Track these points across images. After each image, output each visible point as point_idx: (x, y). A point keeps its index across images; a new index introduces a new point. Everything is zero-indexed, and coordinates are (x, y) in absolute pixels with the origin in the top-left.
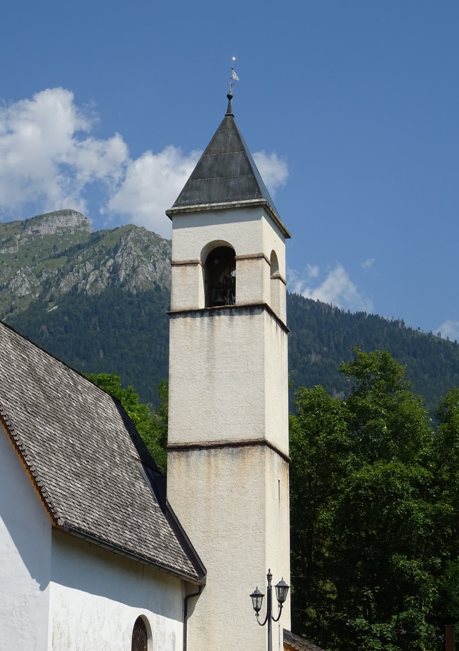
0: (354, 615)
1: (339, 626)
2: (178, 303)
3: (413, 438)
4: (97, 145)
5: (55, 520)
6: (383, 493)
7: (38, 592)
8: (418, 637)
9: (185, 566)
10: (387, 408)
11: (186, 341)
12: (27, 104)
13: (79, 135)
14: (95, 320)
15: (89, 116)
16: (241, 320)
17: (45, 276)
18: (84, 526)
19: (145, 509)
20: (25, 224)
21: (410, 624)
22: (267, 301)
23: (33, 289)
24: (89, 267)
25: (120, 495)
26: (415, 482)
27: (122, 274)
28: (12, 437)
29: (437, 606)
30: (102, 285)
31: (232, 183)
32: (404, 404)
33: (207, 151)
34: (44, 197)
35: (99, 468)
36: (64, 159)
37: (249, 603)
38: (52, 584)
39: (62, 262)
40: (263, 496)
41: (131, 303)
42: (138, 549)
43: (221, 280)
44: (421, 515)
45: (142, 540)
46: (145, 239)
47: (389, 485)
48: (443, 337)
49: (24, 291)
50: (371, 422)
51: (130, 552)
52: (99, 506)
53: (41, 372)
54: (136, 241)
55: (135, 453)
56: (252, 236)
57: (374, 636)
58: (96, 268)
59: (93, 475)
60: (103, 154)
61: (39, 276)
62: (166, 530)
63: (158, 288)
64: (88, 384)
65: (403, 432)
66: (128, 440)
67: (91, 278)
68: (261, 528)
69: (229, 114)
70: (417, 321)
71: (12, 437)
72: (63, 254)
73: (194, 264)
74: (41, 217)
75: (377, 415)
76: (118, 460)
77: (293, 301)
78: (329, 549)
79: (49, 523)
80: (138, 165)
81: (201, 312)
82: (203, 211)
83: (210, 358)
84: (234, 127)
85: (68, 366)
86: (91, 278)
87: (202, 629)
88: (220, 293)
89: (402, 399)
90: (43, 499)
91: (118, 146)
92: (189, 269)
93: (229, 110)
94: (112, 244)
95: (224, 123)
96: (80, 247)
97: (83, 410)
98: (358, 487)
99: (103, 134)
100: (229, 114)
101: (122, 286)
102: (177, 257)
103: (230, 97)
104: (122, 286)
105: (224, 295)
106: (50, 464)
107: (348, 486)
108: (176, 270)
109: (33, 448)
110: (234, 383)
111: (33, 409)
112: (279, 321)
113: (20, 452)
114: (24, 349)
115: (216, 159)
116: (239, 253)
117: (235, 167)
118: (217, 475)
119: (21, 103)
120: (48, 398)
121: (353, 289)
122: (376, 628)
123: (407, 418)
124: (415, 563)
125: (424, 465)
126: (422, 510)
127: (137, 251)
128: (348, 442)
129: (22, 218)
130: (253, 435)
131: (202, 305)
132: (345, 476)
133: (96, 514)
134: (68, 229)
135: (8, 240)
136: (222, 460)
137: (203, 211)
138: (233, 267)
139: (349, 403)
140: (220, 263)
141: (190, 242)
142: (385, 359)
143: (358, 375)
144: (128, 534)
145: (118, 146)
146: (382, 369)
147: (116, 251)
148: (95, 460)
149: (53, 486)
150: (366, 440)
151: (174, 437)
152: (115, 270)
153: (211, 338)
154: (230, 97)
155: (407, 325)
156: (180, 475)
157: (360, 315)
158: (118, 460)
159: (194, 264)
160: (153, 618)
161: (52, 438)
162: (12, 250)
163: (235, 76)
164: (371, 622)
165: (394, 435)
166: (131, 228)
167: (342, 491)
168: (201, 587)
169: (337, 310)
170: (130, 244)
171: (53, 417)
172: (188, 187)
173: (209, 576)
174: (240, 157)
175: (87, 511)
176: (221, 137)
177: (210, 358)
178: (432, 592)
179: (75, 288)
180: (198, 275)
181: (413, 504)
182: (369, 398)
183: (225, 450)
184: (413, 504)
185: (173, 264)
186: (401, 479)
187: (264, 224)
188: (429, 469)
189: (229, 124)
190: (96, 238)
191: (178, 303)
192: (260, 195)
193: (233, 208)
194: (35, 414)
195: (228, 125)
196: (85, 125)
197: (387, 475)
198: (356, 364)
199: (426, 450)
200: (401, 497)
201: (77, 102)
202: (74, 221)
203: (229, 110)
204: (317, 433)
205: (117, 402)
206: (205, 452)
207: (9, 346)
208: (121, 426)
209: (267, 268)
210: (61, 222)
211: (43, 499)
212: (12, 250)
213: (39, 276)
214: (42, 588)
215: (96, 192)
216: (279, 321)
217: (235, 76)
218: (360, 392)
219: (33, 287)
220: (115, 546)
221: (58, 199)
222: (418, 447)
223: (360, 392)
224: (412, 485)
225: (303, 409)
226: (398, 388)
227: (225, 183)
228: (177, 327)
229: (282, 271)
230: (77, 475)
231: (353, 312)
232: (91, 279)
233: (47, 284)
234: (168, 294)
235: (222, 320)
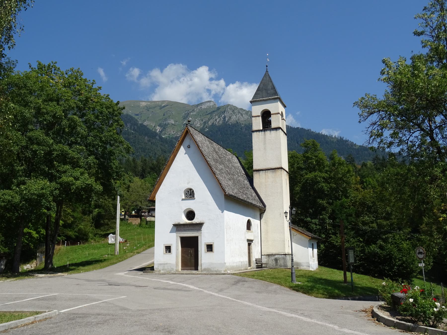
0: (306, 217)
1: (302, 220)
2: (254, 128)
3: (323, 165)
4: (217, 82)
5: (225, 193)
6: (315, 182)
7: (221, 214)
8: (326, 223)
9: (261, 205)
10: (315, 156)
11: (257, 139)
12: (195, 71)
13: (211, 79)
14: (219, 133)
15: (214, 73)
16: (273, 132)
17: (204, 121)
18: (233, 194)
19: (248, 188)
20: (198, 105)
21: (323, 219)
22: (281, 126)
23: (201, 124)
24: (217, 117)
25: (241, 185)
26: (324, 178)
27: (227, 119)
28: (211, 169)
29: (332, 214)
30: (221, 122)
31: (269, 92)
32: (319, 155)
33: (261, 83)
34: (201, 98)
35: (235, 177)
36: (207, 87)
37: (284, 215)
38: (225, 211)
39: (209, 116)
40: (282, 184)
41: (230, 127)
42: (248, 200)
43: (267, 121)
44: (326, 188)
45: (248, 198)
46: (233, 108)
47: (316, 179)
48: (323, 134)
49: (198, 125)
50: (310, 161)
51: (246, 201)
52: (236, 188)
53: (217, 150)
54: (230, 109)
55: (244, 172)
56: (275, 107)
57: (313, 223)
58: (219, 117)
59: (233, 179)
60: (217, 85)
61: (202, 121)
62: (254, 194)
63: (237, 123)
64: (229, 153)
65: (320, 163)
66: (241, 169)
67: (218, 121)
68: (282, 193)
69: (267, 71)
70: (315, 129)
71: (211, 169)
72: (209, 114)
73: (259, 116)
74: (202, 103)
75: (311, 159)
76: (239, 174)
77: (287, 127)
78: (298, 198)
79: (224, 193)
80: (228, 88)
81: (261, 131)
82: (261, 101)
83: (265, 143)
84: (269, 75)
85: (224, 148)
86: (218, 121)
87: (265, 223)
88: (267, 125)
89: (319, 153)
90: (222, 187)
91: (222, 82)
92: (257, 118)
93: (267, 70)
94: (223, 110)
95: (265, 74)
96: (214, 111)
97: (229, 160)
98: (307, 180)
99: (218, 79)
100: (267, 71)
101: (227, 122)
102: (253, 115)
103: (267, 66)
104: (227, 122)
105: (268, 125)
106: (222, 176)
107: (304, 180)
108: (253, 118)
109: (218, 172)
110: (272, 151)
111: (216, 161)
112: (284, 132)
113: (214, 173)
114: (212, 144)
115: (264, 85)
116: (272, 113)
117: (270, 87)
118: (268, 178)
119: (194, 72)
120: (220, 157)
121: (294, 121)
122: (313, 221)
123: (321, 159)
124: (324, 202)
125: (326, 173)
126: (326, 186)
127: (231, 112)
128: (303, 167)
129: (197, 104)
130: (278, 166)
131: (261, 129)
132: (303, 177)
133: (236, 191)
134: (210, 106)
135: (193, 110)
136: (269, 173)
137: (261, 101)
138: (271, 117)
139: (303, 155)
140: (266, 115)
141: (257, 110)
142: (313, 142)
143: (306, 147)
144: (244, 196)
145: (222, 82)
146: (313, 145)
147: (224, 112)
148: (234, 175)
149: (224, 183)
150: (309, 166)
151: (255, 167)
152: (224, 118)
153: (265, 138)
154: (267, 66)
155: (312, 131)
156: (257, 178)
157: (298, 128)
158: (239, 174)
159: (259, 116)
160: (252, 220)
161: (222, 169)
162: (194, 113)
163: (268, 60)
164: (312, 219)
165: (317, 164)
166: (229, 105)
167: (302, 181)
168: (265, 211)
169: (291, 127)
170: (229, 110)
171: (222, 163)
172: (256, 94)
173: (267, 207)
174: (271, 84)
175: (233, 190)
176: (265, 78)
177: (265, 143)
178: (330, 210)
179: (213, 123)
180: (260, 119)
181: (324, 185)
182: (309, 154)
183: (270, 171)
184: (324, 185)
185: (253, 117)
186: (320, 177)
187: (279, 103)
188: (328, 174)
189: (267, 74)
190: (219, 108)
191: (254, 128)
192: (277, 95)
193: (270, 99)
194: (217, 162)
195: (267, 74)
196: (213, 76)
197: (315, 176)
198: (305, 143)
199: (327, 168)
200: (320, 182)
201: (210, 70)
202: (212, 104)
203: (267, 70)
204: (294, 164)
205: (237, 158)
206: (264, 171)
207: (208, 143)
208: (239, 165)
209: (280, 117)
210: (208, 104)
211: (222, 187)
212: (194, 113)
213: (202, 121)
214: (222, 212)
215: (217, 96)
216: (284, 132)
217: (268, 60)
218: (307, 152)
219: (201, 124)
220: (242, 200)
221: (206, 98)
222: (324, 167)
223: (307, 152)
224: (323, 179)
225: (292, 158)
226: (318, 150)
227: (267, 91)
228: (255, 135)
229: (284, 117)
230: (230, 179)
231: (296, 127)
232: (218, 121)
233: (205, 123)
234: (252, 126)
235: (268, 133)
